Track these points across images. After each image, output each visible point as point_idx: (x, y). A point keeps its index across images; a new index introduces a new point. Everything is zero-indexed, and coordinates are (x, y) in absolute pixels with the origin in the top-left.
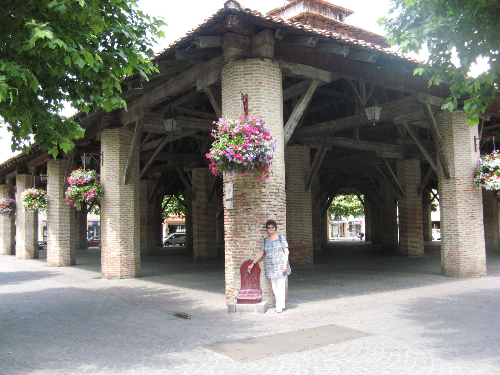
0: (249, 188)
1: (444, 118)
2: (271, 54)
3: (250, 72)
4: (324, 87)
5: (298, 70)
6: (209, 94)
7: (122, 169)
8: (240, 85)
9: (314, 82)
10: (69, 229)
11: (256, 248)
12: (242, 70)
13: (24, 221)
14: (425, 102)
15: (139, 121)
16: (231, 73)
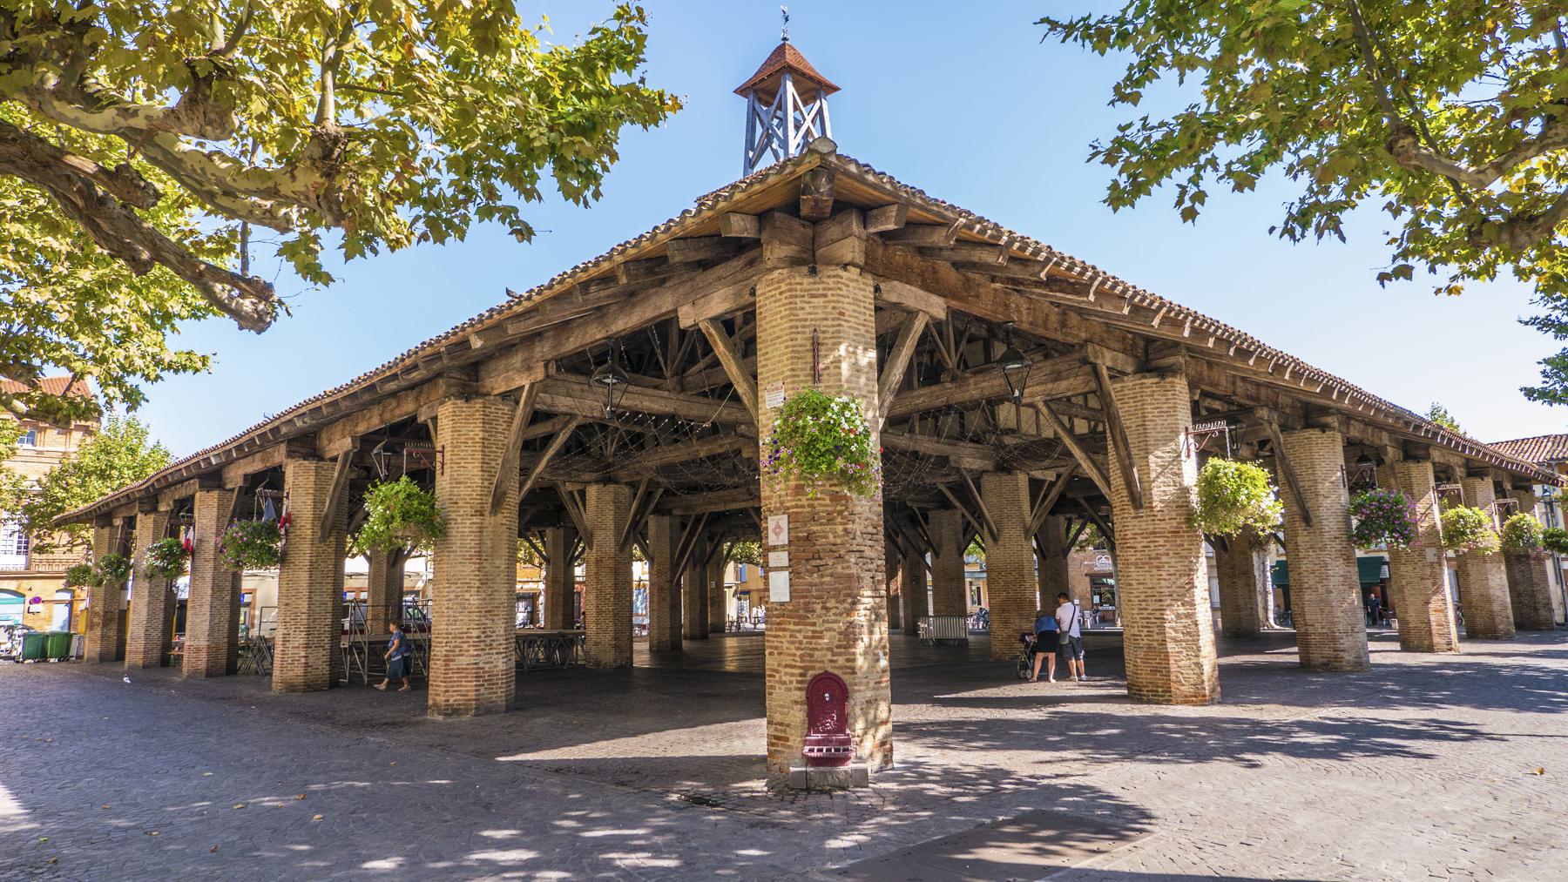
0: (822, 524)
1: (1126, 392)
2: (860, 259)
3: (821, 292)
4: (935, 328)
5: (904, 293)
6: (711, 334)
7: (486, 483)
8: (801, 317)
9: (921, 315)
10: (330, 609)
11: (838, 647)
12: (805, 286)
13: (210, 592)
14: (1099, 362)
15: (532, 385)
16: (781, 293)
